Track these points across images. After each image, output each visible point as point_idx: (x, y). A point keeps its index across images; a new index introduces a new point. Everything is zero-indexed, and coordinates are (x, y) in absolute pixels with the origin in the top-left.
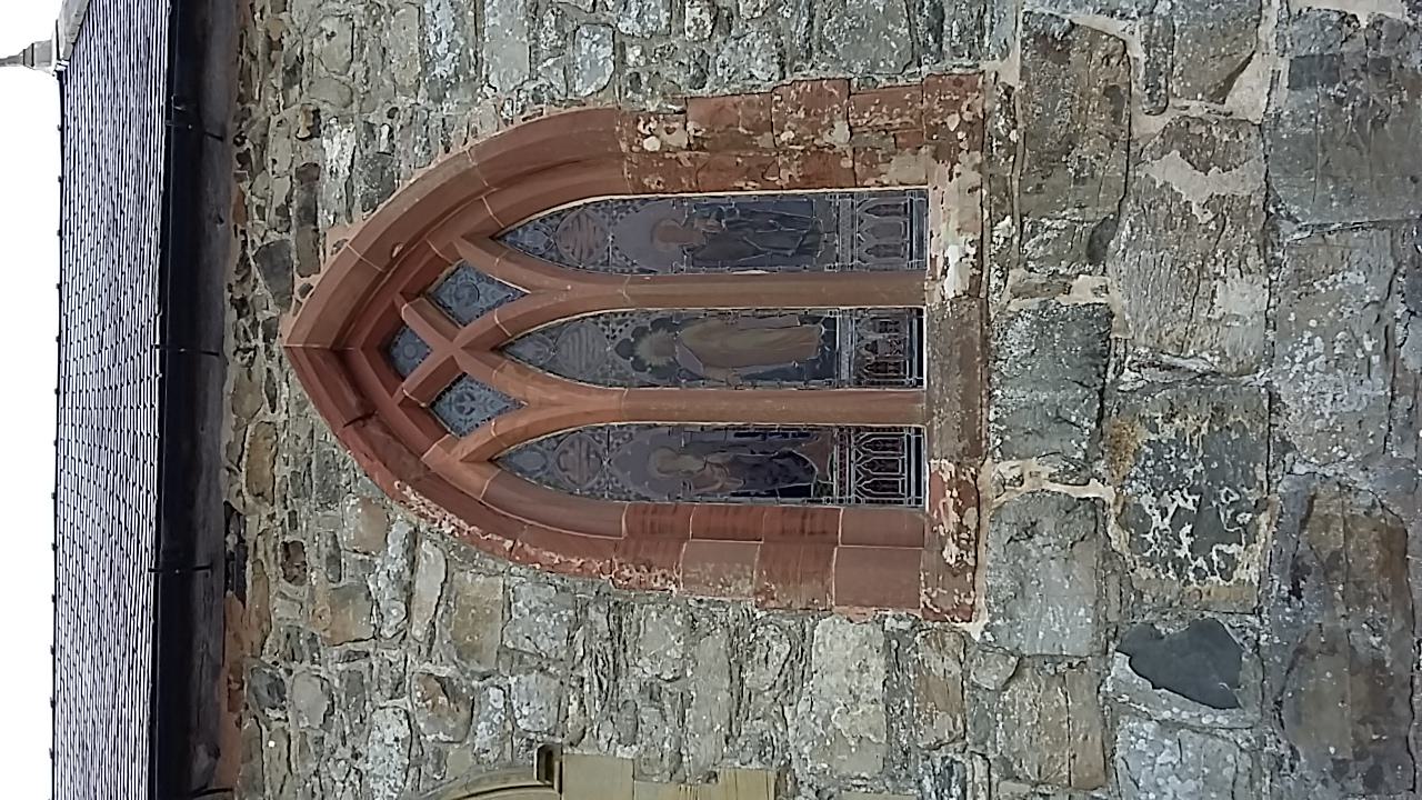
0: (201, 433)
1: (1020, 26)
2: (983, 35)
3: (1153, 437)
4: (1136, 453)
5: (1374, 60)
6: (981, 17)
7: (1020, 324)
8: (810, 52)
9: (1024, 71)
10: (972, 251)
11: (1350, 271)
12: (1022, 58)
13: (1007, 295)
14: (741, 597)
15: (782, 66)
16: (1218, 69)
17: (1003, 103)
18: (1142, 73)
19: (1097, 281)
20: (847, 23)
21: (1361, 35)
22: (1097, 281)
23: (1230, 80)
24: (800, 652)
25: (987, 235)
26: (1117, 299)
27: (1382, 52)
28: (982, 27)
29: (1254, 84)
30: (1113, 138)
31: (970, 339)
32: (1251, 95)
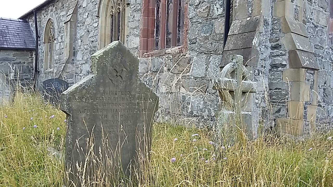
0: (29, 52)
1: (192, 56)
2: (191, 50)
3: (153, 79)
4: (151, 77)
5: (184, 107)
6: (193, 50)
7: (162, 60)
8: (192, 23)
9: (187, 57)
10: (169, 53)
11: (274, 119)
12: (188, 57)
13: (165, 58)
14: (141, 27)
15: (190, 19)
16: (185, 86)
17: (183, 55)
18: (185, 75)
19: (166, 70)
20: (195, 28)
21: (187, 106)
22: (166, 70)
23: (184, 87)
24: (137, 36)
25: (171, 54)
26: (164, 73)
27: (185, 109)
28: (192, 50)
29: (183, 91)
30: (179, 71)
31: (161, 54)
32: (183, 90)
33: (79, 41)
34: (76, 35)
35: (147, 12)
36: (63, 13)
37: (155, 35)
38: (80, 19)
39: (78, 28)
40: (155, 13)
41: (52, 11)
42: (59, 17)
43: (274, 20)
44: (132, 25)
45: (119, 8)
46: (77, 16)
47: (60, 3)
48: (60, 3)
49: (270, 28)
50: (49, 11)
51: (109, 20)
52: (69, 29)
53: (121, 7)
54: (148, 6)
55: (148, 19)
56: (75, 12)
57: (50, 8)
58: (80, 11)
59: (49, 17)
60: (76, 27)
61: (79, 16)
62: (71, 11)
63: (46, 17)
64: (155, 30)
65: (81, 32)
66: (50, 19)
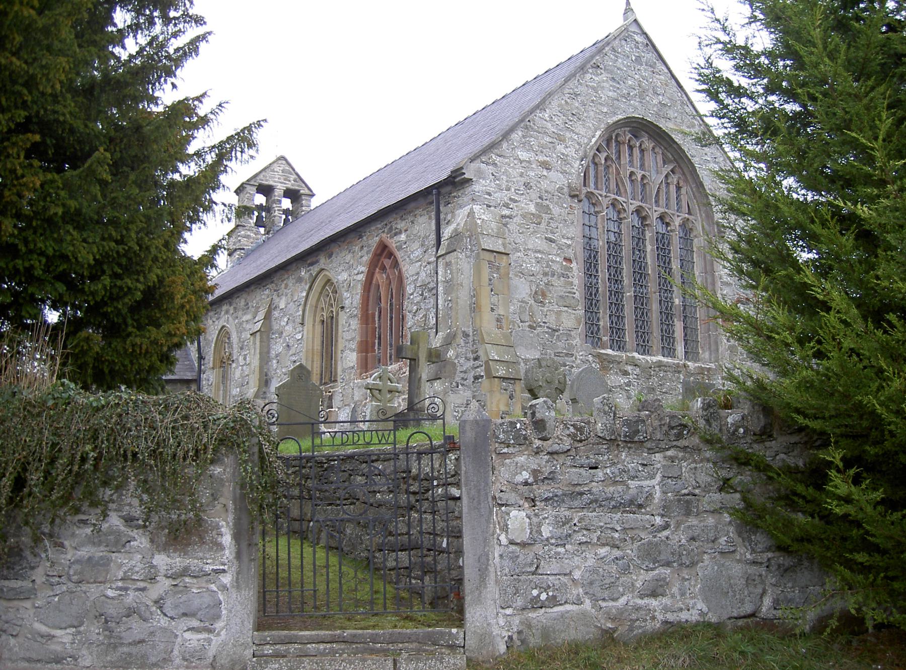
14: (358, 339)
33: (275, 361)
34: (268, 352)
35: (366, 318)
36: (248, 317)
37: (376, 348)
38: (276, 327)
39: (273, 341)
40: (377, 319)
41: (227, 312)
42: (241, 324)
43: (475, 331)
44: (348, 336)
45: (332, 312)
46: (270, 322)
47: (243, 300)
48: (243, 300)
49: (471, 339)
50: (223, 313)
51: (318, 328)
52: (258, 343)
53: (334, 310)
54: (367, 310)
55: (367, 328)
56: (268, 316)
57: (225, 308)
58: (276, 314)
59: (222, 322)
60: (269, 339)
61: (274, 323)
62: (261, 315)
63: (216, 323)
64: (377, 341)
65: (278, 348)
66: (223, 327)
